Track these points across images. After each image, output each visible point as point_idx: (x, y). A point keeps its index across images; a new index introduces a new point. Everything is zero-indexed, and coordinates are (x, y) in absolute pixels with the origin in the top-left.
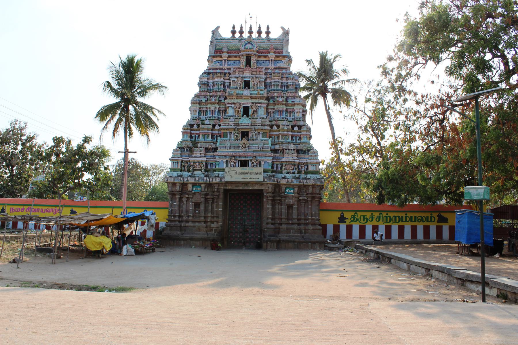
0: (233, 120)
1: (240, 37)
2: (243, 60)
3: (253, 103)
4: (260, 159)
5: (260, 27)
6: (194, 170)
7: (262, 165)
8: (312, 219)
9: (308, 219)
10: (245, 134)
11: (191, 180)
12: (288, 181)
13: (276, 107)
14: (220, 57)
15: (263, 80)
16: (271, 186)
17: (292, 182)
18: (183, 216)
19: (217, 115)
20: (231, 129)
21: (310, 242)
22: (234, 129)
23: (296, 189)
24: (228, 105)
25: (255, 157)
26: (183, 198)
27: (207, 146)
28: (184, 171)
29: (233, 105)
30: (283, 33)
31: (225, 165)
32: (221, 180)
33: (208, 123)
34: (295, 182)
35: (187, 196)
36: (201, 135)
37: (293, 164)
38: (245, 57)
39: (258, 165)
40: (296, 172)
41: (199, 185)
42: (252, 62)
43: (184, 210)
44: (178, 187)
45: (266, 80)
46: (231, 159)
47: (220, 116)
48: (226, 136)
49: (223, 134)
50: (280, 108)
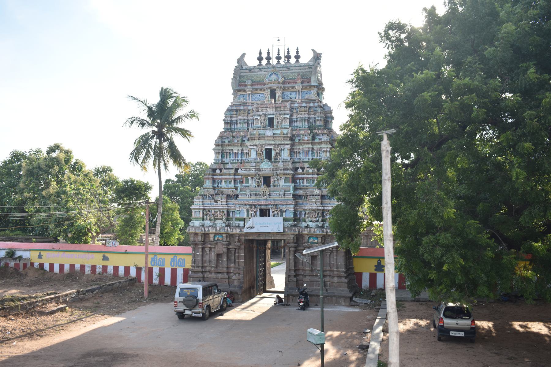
0: (254, 164)
1: (267, 64)
2: (267, 94)
3: (275, 145)
4: (281, 207)
5: (288, 52)
6: (215, 220)
7: (284, 214)
8: (337, 271)
9: (333, 271)
10: (267, 181)
11: (212, 230)
12: (310, 231)
13: (301, 147)
14: (244, 90)
15: (288, 116)
16: (293, 236)
17: (314, 232)
18: (206, 267)
19: (240, 158)
20: (252, 175)
21: (334, 296)
22: (256, 175)
23: (320, 239)
24: (250, 147)
25: (276, 205)
26: (205, 247)
27: (229, 193)
28: (207, 219)
29: (255, 147)
30: (314, 57)
31: (246, 214)
32: (241, 231)
33: (231, 167)
34: (318, 232)
35: (209, 246)
36: (223, 181)
37: (316, 211)
38: (269, 90)
39: (280, 214)
40: (320, 220)
41: (221, 234)
42: (277, 96)
43: (208, 260)
44: (200, 238)
45: (291, 115)
46: (251, 208)
47: (244, 159)
48: (247, 181)
49: (245, 179)
50: (306, 147)
